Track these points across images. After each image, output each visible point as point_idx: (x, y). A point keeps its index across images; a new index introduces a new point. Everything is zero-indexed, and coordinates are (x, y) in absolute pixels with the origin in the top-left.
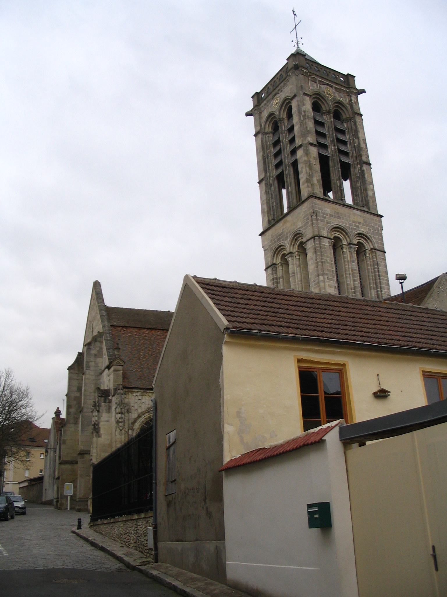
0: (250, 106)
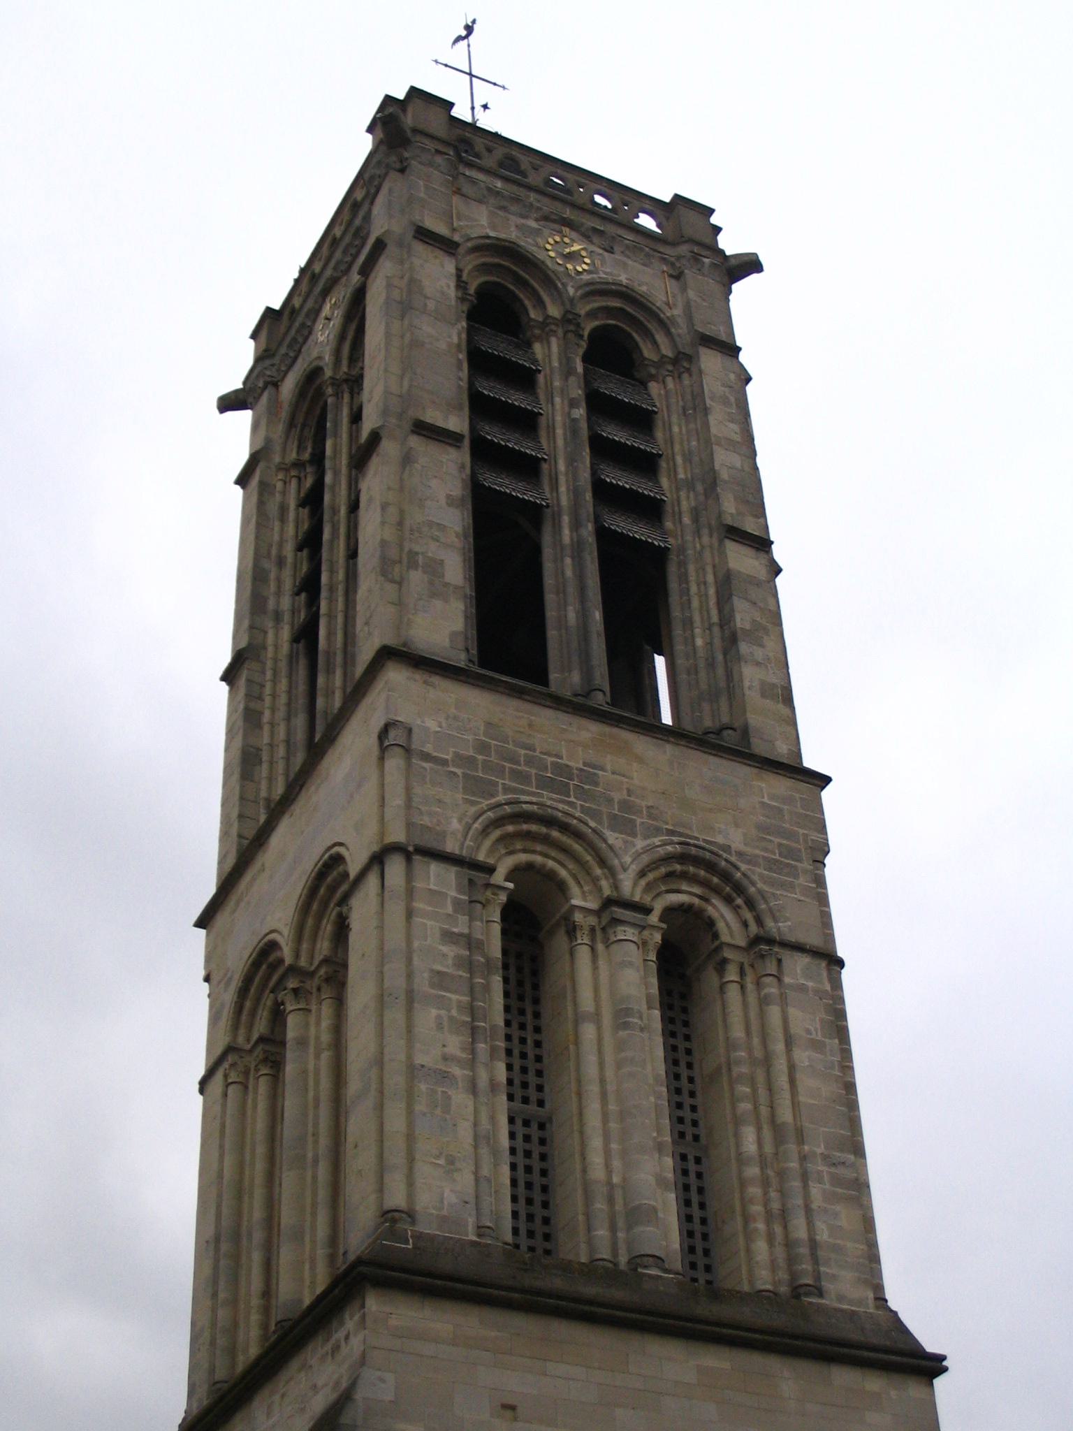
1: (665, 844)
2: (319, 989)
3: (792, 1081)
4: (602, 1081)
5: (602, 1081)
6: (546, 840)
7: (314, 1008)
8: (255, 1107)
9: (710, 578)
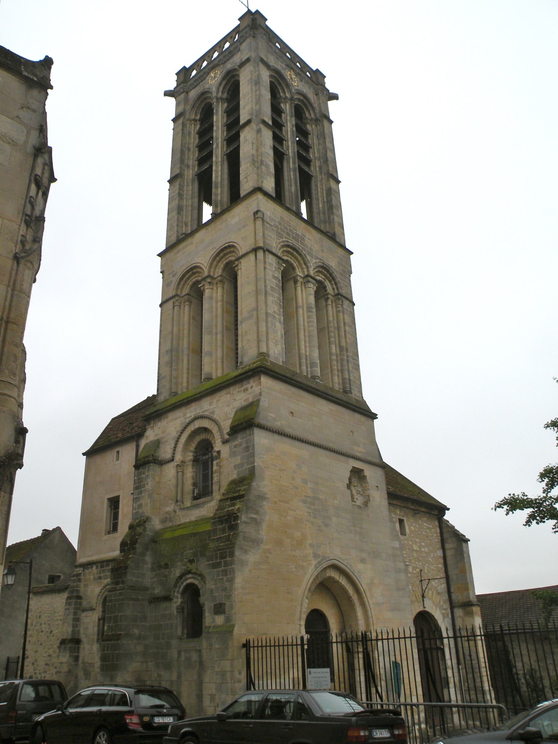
0: (172, 85)
2: (217, 283)
3: (345, 335)
4: (304, 326)
5: (304, 326)
7: (215, 288)
8: (184, 313)
9: (324, 188)
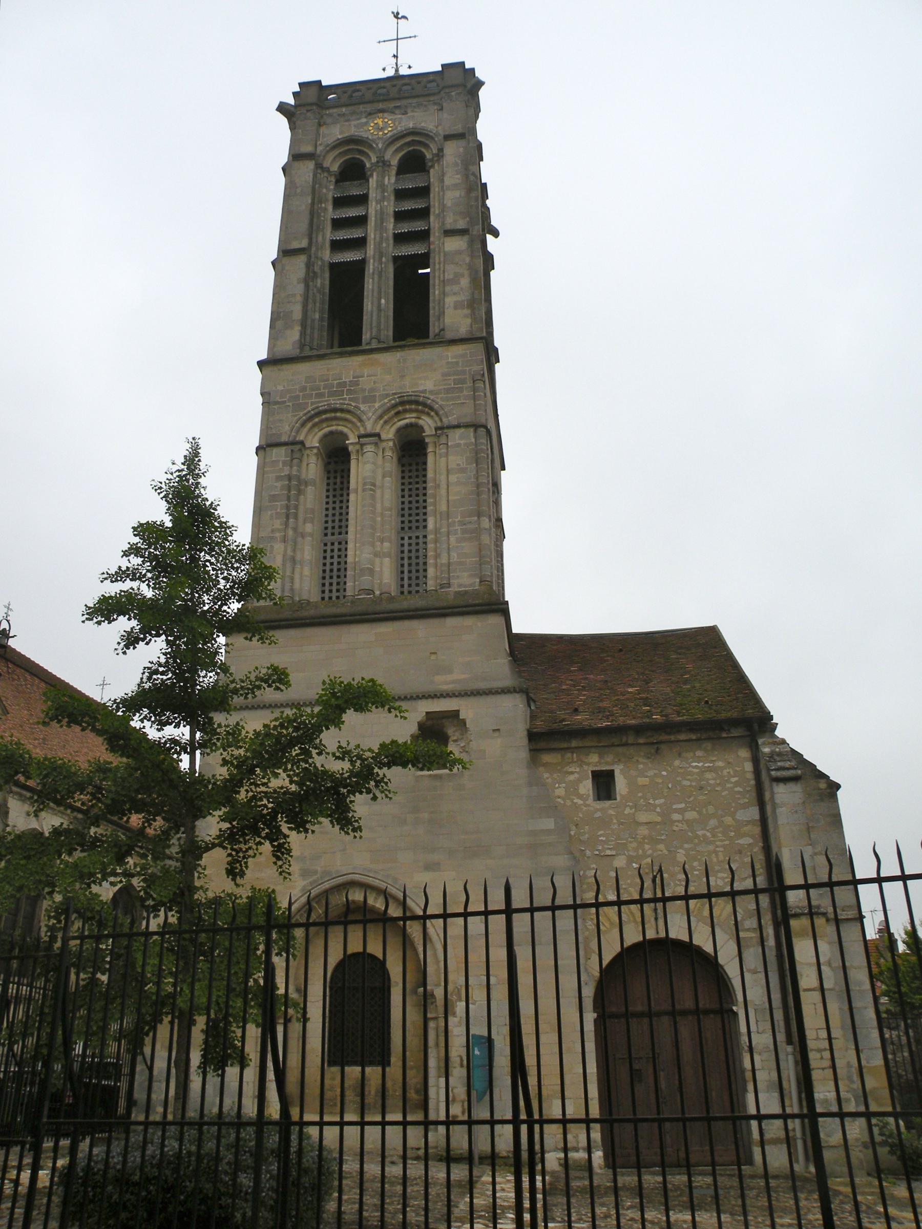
1: (390, 401)
6: (336, 418)
